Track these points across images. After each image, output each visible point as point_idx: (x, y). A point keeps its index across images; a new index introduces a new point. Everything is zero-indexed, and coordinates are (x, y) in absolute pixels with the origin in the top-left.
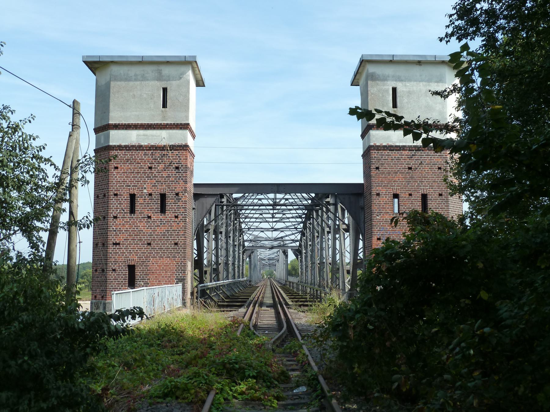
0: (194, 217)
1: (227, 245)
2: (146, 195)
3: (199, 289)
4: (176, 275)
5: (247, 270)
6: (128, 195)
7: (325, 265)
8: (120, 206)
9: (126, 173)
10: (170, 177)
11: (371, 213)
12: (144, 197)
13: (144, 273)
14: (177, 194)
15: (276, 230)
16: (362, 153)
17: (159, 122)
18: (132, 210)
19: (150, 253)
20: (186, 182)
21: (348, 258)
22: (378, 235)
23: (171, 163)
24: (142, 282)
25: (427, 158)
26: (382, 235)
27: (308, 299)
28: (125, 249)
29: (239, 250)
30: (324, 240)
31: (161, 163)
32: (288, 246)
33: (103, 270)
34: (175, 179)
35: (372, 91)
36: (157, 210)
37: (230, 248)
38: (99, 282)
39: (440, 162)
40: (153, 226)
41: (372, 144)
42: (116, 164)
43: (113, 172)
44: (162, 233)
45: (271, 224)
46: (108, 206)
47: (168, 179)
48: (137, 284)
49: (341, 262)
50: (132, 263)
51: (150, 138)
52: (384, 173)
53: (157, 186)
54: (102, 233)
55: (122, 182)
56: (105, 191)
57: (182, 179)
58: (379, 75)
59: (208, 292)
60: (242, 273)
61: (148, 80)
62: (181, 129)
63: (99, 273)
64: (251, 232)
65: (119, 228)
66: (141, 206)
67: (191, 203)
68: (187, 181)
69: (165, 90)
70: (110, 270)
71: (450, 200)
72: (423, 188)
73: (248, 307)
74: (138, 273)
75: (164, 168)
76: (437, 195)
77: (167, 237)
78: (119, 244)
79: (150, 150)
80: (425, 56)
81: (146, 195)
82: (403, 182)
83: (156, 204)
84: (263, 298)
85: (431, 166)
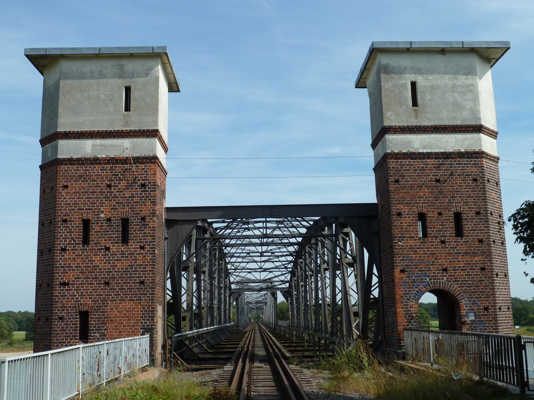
0: (166, 249)
1: (211, 287)
2: (104, 220)
3: (174, 340)
4: (142, 323)
5: (234, 314)
6: (80, 221)
7: (309, 307)
8: (70, 235)
9: (79, 193)
10: (135, 197)
11: (392, 237)
12: (101, 223)
14: (143, 219)
15: (265, 270)
17: (120, 129)
18: (86, 241)
19: (108, 295)
20: (154, 203)
21: (354, 298)
22: (401, 266)
23: (135, 180)
24: (98, 333)
25: (459, 167)
26: (406, 265)
27: (294, 341)
28: (75, 290)
29: (225, 293)
30: (308, 283)
31: (122, 180)
32: (277, 288)
33: (47, 319)
34: (140, 200)
35: (386, 87)
36: (118, 240)
37: (215, 290)
39: (476, 172)
40: (112, 260)
41: (389, 151)
42: (65, 182)
43: (61, 193)
44: (123, 269)
45: (259, 264)
46: (54, 236)
47: (131, 200)
48: (91, 336)
49: (322, 303)
50: (85, 309)
51: (109, 148)
52: (405, 187)
53: (117, 209)
54: (47, 271)
55: (73, 204)
56: (51, 217)
57: (150, 199)
58: (394, 68)
59: (187, 342)
60: (229, 317)
61: (107, 77)
62: (148, 136)
63: (42, 322)
64: (237, 274)
65: (69, 264)
66: (97, 235)
67: (162, 232)
68: (155, 202)
69: (128, 90)
70: (56, 319)
71: (490, 219)
72: (456, 206)
74: (92, 322)
75: (126, 186)
76: (473, 213)
77: (130, 274)
78: (68, 284)
79: (108, 163)
80: (450, 42)
81: (104, 220)
82: (430, 197)
83: (116, 231)
84: (253, 347)
85: (464, 178)
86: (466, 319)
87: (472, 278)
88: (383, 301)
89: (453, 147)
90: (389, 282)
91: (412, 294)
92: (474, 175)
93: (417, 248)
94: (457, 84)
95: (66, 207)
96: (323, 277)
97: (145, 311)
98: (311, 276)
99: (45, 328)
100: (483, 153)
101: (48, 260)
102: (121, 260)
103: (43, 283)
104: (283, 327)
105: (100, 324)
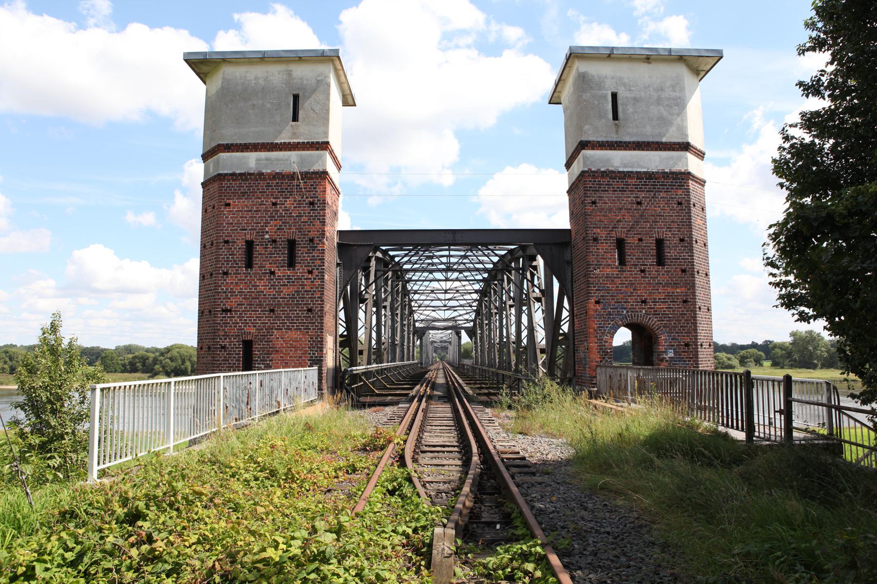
2: (269, 242)
4: (310, 354)
5: (417, 353)
9: (242, 211)
10: (302, 216)
13: (265, 352)
14: (311, 240)
16: (567, 188)
17: (287, 141)
21: (541, 335)
22: (596, 297)
26: (602, 296)
38: (204, 363)
45: (443, 302)
50: (249, 338)
54: (209, 296)
64: (421, 312)
65: (231, 289)
66: (262, 257)
73: (422, 386)
78: (230, 311)
81: (269, 242)
82: (630, 222)
83: (282, 254)
86: (665, 356)
87: (673, 311)
88: (574, 336)
89: (657, 167)
90: (581, 314)
91: (607, 327)
92: (679, 198)
93: (614, 278)
94: (663, 96)
95: (228, 227)
96: (509, 313)
97: (313, 341)
98: (496, 313)
99: (207, 357)
100: (689, 173)
101: (209, 284)
102: (287, 285)
103: (205, 309)
104: (467, 365)
105: (265, 354)
